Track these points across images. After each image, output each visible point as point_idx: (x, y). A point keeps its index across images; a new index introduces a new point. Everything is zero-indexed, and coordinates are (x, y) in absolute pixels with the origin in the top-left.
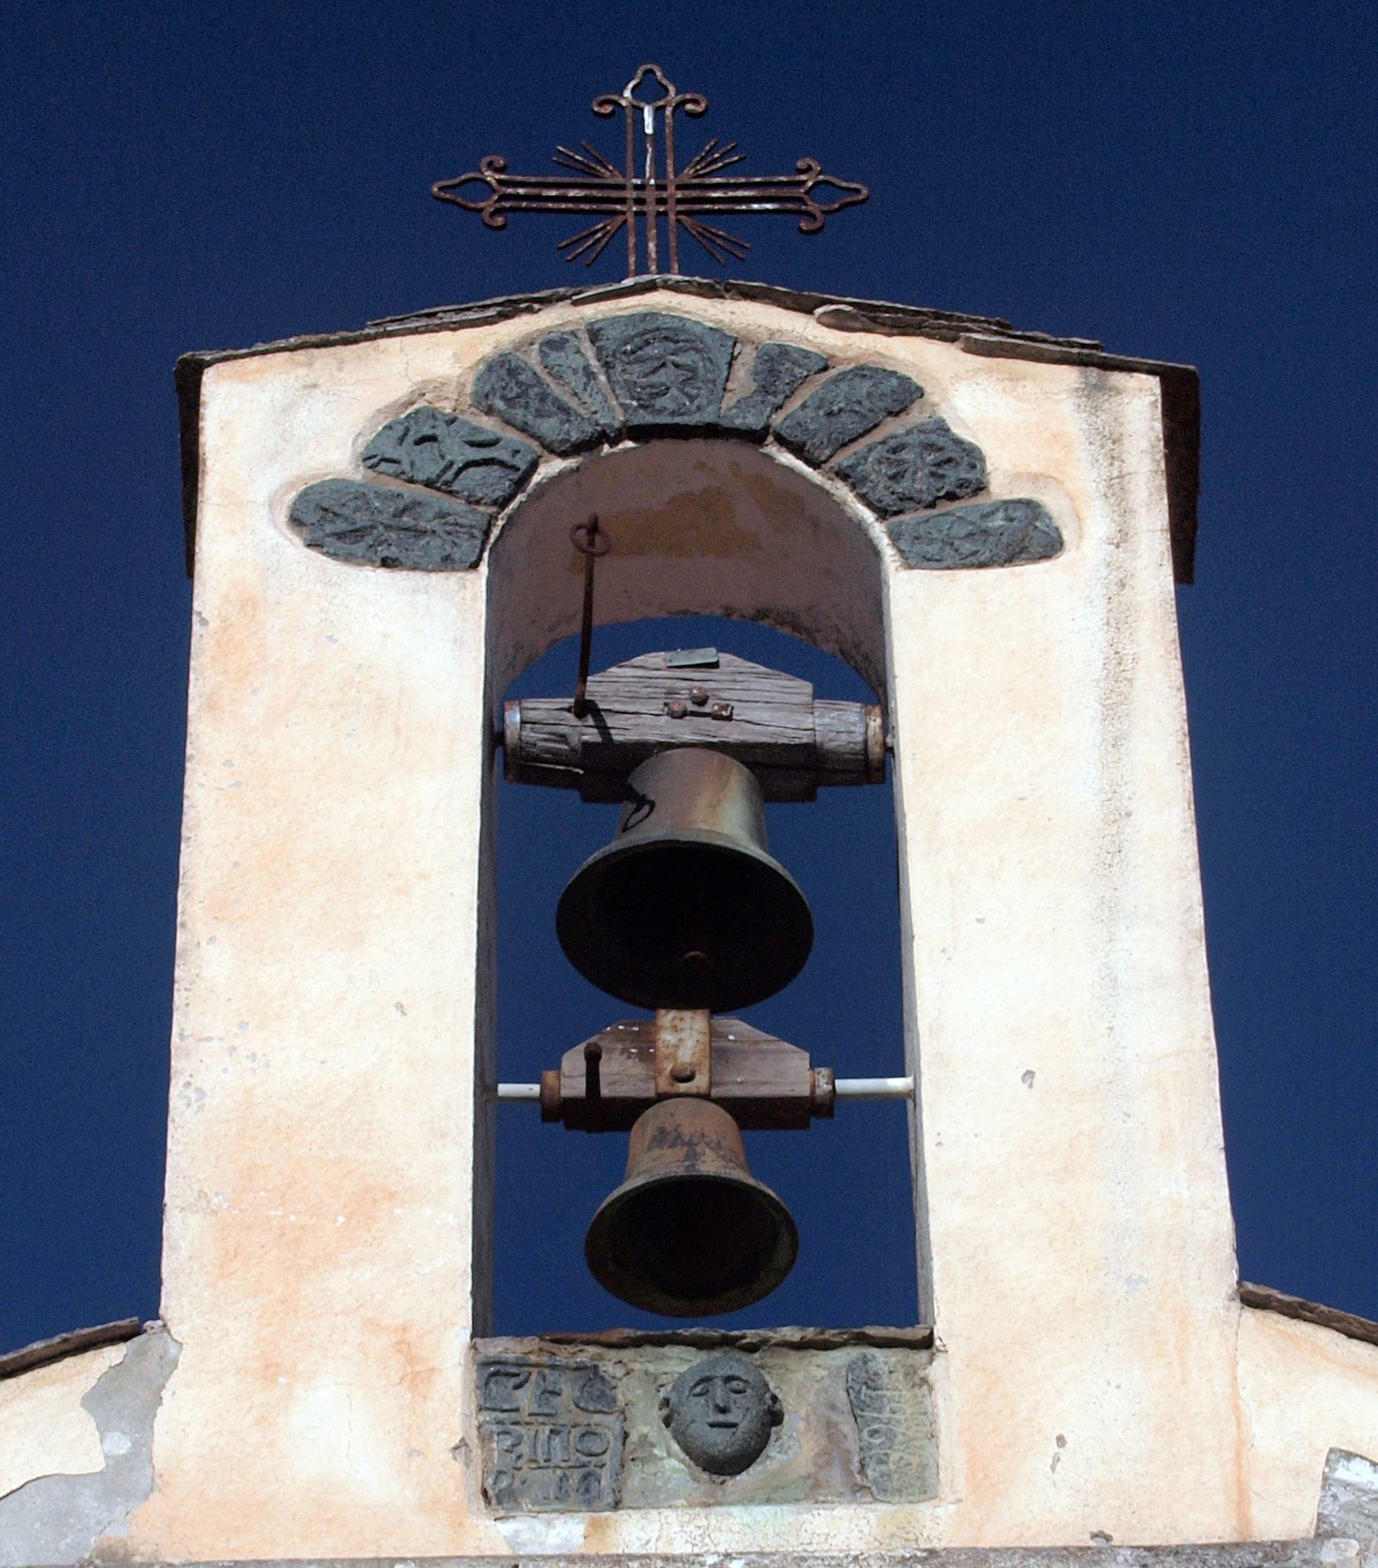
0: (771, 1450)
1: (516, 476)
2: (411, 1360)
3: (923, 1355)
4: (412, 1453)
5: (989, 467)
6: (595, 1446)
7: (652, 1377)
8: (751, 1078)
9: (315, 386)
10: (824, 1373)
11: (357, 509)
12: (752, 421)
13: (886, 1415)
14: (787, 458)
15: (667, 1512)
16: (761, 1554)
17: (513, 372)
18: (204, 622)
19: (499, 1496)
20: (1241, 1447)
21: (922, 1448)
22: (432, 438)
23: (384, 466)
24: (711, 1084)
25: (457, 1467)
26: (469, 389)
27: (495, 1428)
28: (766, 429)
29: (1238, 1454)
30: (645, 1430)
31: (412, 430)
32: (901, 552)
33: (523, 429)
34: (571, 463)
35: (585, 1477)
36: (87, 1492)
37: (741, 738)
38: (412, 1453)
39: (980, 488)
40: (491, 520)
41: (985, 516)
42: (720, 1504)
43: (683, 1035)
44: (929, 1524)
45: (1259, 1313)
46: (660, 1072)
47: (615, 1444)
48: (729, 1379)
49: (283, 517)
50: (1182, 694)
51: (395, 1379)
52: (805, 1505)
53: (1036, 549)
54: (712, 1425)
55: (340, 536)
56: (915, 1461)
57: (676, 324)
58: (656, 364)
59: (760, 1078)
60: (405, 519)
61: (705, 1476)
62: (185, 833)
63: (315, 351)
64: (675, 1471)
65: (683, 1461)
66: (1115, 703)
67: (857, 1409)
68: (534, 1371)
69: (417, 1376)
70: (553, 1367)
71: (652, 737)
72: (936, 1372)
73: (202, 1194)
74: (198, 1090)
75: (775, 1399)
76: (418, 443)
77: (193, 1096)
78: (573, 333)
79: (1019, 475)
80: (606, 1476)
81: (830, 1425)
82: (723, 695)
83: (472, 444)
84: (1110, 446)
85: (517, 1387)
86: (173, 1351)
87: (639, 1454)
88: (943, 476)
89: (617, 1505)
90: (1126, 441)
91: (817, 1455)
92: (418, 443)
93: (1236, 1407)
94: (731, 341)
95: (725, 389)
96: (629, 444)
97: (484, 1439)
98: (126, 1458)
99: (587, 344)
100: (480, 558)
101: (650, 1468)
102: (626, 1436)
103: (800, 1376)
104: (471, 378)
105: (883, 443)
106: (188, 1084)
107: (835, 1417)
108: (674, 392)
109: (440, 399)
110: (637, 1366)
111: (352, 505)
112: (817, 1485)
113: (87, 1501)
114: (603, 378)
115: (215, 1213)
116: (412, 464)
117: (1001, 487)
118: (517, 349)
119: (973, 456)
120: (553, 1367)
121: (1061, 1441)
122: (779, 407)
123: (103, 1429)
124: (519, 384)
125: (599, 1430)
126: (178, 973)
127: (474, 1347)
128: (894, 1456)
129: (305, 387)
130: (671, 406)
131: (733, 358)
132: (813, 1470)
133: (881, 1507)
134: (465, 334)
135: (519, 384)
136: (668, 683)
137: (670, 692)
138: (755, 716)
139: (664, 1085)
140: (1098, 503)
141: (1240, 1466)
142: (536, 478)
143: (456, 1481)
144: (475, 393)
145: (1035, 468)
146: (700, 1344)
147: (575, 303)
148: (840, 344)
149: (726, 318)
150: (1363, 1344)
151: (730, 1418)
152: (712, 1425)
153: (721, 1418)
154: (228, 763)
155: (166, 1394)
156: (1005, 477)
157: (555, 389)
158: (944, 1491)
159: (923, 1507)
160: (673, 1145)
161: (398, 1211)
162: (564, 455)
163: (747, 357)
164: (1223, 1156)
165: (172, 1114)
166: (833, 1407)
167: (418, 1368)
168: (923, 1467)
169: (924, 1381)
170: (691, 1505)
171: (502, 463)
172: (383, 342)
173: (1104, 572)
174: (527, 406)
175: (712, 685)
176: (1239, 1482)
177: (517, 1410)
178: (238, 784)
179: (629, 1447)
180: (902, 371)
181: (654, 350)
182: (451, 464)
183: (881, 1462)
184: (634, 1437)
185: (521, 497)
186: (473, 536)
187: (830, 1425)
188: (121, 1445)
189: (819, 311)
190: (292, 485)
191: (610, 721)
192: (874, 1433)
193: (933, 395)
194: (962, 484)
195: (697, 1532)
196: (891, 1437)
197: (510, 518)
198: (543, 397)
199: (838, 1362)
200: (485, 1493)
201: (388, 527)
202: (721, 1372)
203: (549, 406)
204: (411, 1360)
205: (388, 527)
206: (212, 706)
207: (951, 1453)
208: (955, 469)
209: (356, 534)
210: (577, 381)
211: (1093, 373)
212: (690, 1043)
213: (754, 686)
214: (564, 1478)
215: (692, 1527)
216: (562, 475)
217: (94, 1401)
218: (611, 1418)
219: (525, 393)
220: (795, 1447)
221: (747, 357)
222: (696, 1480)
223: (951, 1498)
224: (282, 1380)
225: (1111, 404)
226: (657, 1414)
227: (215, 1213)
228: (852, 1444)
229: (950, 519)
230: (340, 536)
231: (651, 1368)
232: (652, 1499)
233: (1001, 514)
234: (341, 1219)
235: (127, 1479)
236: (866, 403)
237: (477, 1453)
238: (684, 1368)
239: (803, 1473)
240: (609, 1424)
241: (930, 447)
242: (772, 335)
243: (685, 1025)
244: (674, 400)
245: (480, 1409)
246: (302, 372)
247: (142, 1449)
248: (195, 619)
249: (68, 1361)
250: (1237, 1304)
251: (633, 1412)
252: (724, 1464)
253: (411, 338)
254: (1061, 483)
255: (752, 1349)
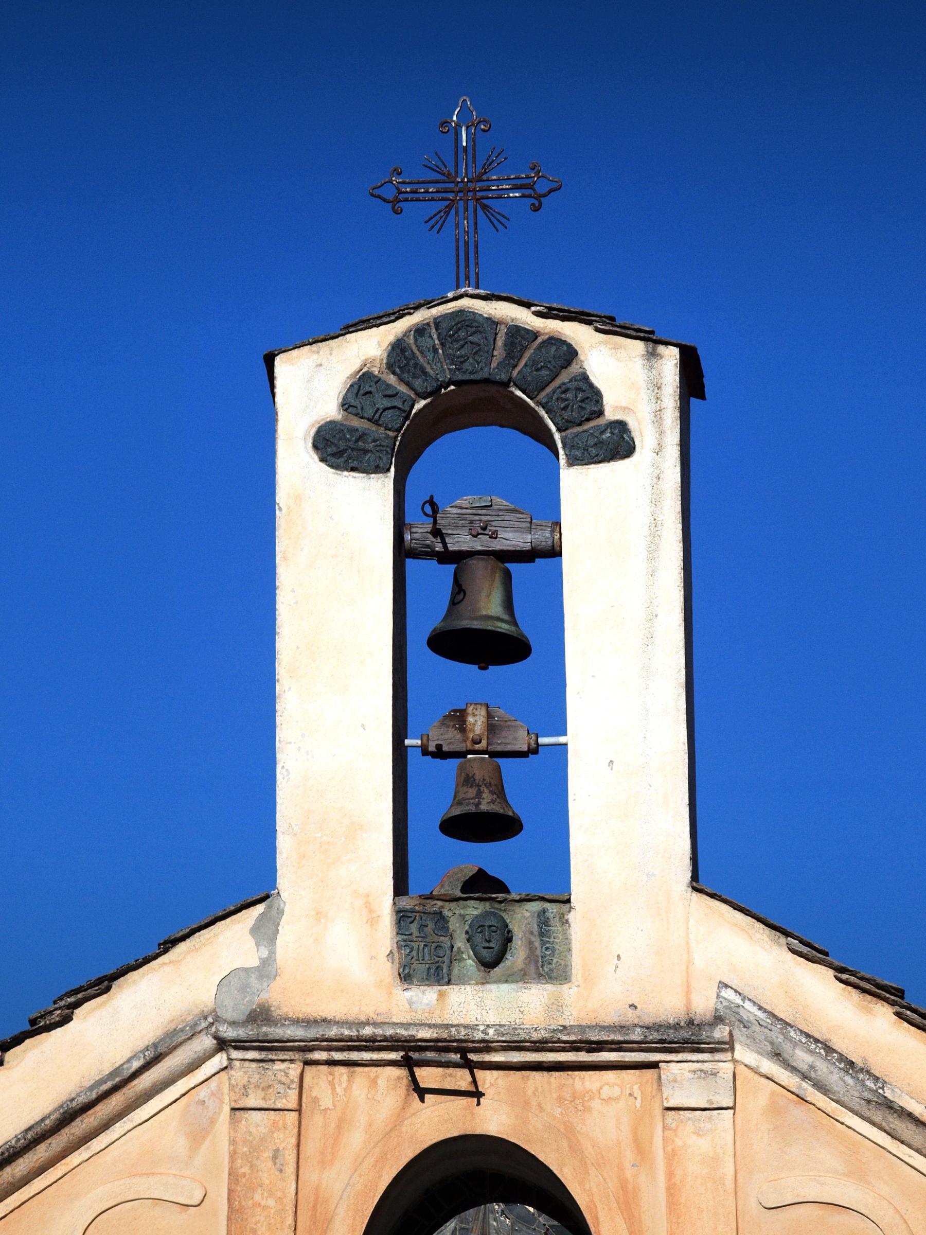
0: (508, 956)
1: (404, 415)
2: (371, 911)
3: (565, 907)
4: (372, 958)
5: (605, 403)
6: (441, 953)
7: (463, 916)
8: (504, 741)
9: (321, 365)
10: (529, 914)
11: (340, 439)
12: (504, 377)
13: (552, 940)
14: (519, 393)
15: (468, 987)
16: (500, 1025)
17: (403, 350)
18: (280, 509)
19: (406, 977)
20: (689, 963)
21: (566, 956)
22: (370, 392)
23: (350, 409)
24: (488, 744)
25: (389, 964)
26: (385, 361)
27: (402, 943)
28: (510, 380)
29: (688, 967)
30: (459, 944)
31: (362, 388)
32: (566, 455)
33: (408, 384)
34: (428, 400)
35: (437, 968)
36: (253, 976)
37: (501, 548)
38: (372, 958)
39: (601, 413)
40: (396, 437)
41: (602, 433)
42: (488, 983)
43: (477, 718)
44: (567, 998)
45: (699, 895)
46: (467, 738)
47: (448, 952)
48: (490, 926)
49: (310, 445)
50: (681, 545)
51: (365, 921)
52: (520, 984)
53: (622, 450)
54: (484, 948)
55: (333, 455)
56: (563, 963)
57: (472, 317)
58: (462, 343)
59: (507, 741)
60: (360, 443)
61: (483, 968)
62: (277, 630)
63: (320, 344)
64: (471, 966)
65: (473, 960)
66: (653, 554)
67: (542, 934)
68: (418, 915)
69: (373, 921)
70: (424, 913)
71: (464, 548)
72: (571, 917)
73: (290, 826)
74: (287, 770)
75: (509, 931)
76: (365, 394)
77: (286, 774)
78: (428, 324)
79: (617, 407)
80: (445, 967)
81: (531, 943)
82: (493, 524)
83: (426, 222)
84: (656, 391)
85: (411, 923)
86: (282, 905)
87: (458, 957)
88: (585, 408)
89: (449, 983)
90: (663, 387)
91: (526, 959)
92: (365, 394)
93: (688, 943)
94: (493, 323)
95: (493, 356)
96: (452, 387)
97: (399, 947)
98: (267, 959)
99: (434, 330)
100: (390, 468)
101: (462, 965)
102: (452, 947)
103: (520, 915)
104: (385, 355)
105: (559, 387)
106: (283, 767)
107: (533, 939)
108: (471, 360)
109: (373, 366)
110: (457, 912)
111: (338, 436)
112: (525, 975)
113: (253, 980)
114: (440, 351)
115: (295, 835)
116: (362, 409)
117: (610, 414)
118: (404, 335)
119: (596, 396)
120: (424, 913)
121: (619, 956)
122: (515, 366)
123: (258, 945)
124: (406, 358)
125: (442, 945)
126: (278, 707)
127: (394, 904)
128: (555, 961)
129: (317, 366)
130: (470, 368)
131: (496, 334)
132: (523, 966)
133: (549, 987)
134: (382, 328)
135: (406, 358)
136: (472, 517)
137: (472, 522)
138: (506, 535)
139: (469, 745)
140: (650, 426)
141: (688, 972)
142: (414, 411)
143: (388, 970)
144: (387, 364)
145: (624, 404)
146: (480, 899)
147: (428, 308)
148: (542, 326)
149: (492, 312)
150: (739, 913)
151: (492, 945)
152: (484, 948)
153: (487, 945)
154: (293, 591)
155: (280, 928)
156: (613, 407)
157: (421, 359)
158: (574, 979)
159: (566, 986)
160: (471, 787)
161: (364, 835)
162: (425, 399)
163: (503, 330)
164: (688, 809)
165: (278, 783)
166: (532, 933)
167: (374, 915)
168: (566, 966)
169: (567, 921)
170: (477, 984)
171: (399, 408)
172: (348, 336)
173: (651, 469)
174: (409, 372)
175: (489, 518)
176: (688, 982)
177: (411, 935)
178: (297, 602)
179: (454, 953)
180: (569, 341)
181: (462, 334)
182: (378, 409)
183: (550, 964)
184: (455, 949)
185: (407, 423)
186: (387, 452)
187: (531, 943)
188: (264, 953)
189: (533, 309)
190: (313, 425)
191: (447, 540)
192: (547, 948)
193: (582, 356)
194: (593, 413)
195: (479, 1000)
196: (553, 950)
197: (403, 434)
198: (416, 365)
199: (534, 909)
200: (399, 974)
201: (353, 449)
202: (487, 923)
203: (418, 372)
204: (371, 911)
205: (353, 449)
206: (285, 558)
207: (577, 961)
208: (589, 397)
209: (338, 454)
210: (430, 356)
211: (651, 345)
212: (479, 723)
213: (507, 518)
214: (429, 969)
215: (476, 997)
216: (425, 406)
217: (255, 930)
218: (447, 939)
219: (407, 364)
220: (517, 955)
221: (503, 330)
222: (479, 970)
223: (576, 984)
224: (323, 920)
225: (658, 364)
226: (464, 936)
227: (295, 835)
228: (538, 952)
229: (586, 434)
230: (333, 455)
231: (462, 912)
232: (463, 980)
233: (609, 430)
234: (343, 839)
235: (266, 969)
236: (553, 362)
237: (396, 955)
238: (476, 913)
239: (520, 968)
240: (445, 940)
241: (579, 389)
242: (513, 320)
243: (477, 713)
244: (471, 364)
245: (397, 934)
246: (315, 356)
247: (272, 953)
248: (277, 507)
249: (244, 912)
250: (690, 889)
251: (455, 935)
252: (491, 962)
253: (359, 333)
254: (635, 413)
255: (501, 902)
